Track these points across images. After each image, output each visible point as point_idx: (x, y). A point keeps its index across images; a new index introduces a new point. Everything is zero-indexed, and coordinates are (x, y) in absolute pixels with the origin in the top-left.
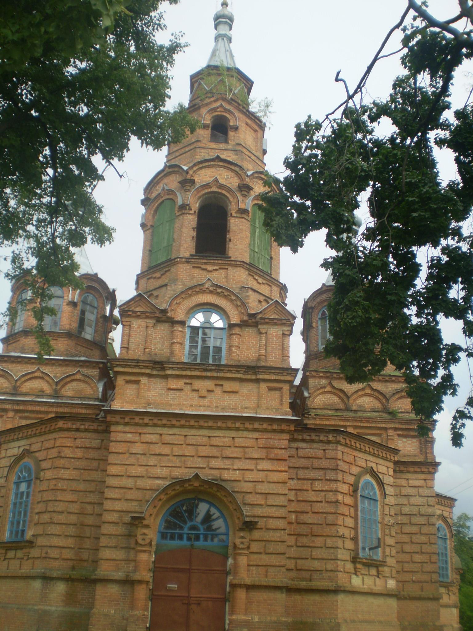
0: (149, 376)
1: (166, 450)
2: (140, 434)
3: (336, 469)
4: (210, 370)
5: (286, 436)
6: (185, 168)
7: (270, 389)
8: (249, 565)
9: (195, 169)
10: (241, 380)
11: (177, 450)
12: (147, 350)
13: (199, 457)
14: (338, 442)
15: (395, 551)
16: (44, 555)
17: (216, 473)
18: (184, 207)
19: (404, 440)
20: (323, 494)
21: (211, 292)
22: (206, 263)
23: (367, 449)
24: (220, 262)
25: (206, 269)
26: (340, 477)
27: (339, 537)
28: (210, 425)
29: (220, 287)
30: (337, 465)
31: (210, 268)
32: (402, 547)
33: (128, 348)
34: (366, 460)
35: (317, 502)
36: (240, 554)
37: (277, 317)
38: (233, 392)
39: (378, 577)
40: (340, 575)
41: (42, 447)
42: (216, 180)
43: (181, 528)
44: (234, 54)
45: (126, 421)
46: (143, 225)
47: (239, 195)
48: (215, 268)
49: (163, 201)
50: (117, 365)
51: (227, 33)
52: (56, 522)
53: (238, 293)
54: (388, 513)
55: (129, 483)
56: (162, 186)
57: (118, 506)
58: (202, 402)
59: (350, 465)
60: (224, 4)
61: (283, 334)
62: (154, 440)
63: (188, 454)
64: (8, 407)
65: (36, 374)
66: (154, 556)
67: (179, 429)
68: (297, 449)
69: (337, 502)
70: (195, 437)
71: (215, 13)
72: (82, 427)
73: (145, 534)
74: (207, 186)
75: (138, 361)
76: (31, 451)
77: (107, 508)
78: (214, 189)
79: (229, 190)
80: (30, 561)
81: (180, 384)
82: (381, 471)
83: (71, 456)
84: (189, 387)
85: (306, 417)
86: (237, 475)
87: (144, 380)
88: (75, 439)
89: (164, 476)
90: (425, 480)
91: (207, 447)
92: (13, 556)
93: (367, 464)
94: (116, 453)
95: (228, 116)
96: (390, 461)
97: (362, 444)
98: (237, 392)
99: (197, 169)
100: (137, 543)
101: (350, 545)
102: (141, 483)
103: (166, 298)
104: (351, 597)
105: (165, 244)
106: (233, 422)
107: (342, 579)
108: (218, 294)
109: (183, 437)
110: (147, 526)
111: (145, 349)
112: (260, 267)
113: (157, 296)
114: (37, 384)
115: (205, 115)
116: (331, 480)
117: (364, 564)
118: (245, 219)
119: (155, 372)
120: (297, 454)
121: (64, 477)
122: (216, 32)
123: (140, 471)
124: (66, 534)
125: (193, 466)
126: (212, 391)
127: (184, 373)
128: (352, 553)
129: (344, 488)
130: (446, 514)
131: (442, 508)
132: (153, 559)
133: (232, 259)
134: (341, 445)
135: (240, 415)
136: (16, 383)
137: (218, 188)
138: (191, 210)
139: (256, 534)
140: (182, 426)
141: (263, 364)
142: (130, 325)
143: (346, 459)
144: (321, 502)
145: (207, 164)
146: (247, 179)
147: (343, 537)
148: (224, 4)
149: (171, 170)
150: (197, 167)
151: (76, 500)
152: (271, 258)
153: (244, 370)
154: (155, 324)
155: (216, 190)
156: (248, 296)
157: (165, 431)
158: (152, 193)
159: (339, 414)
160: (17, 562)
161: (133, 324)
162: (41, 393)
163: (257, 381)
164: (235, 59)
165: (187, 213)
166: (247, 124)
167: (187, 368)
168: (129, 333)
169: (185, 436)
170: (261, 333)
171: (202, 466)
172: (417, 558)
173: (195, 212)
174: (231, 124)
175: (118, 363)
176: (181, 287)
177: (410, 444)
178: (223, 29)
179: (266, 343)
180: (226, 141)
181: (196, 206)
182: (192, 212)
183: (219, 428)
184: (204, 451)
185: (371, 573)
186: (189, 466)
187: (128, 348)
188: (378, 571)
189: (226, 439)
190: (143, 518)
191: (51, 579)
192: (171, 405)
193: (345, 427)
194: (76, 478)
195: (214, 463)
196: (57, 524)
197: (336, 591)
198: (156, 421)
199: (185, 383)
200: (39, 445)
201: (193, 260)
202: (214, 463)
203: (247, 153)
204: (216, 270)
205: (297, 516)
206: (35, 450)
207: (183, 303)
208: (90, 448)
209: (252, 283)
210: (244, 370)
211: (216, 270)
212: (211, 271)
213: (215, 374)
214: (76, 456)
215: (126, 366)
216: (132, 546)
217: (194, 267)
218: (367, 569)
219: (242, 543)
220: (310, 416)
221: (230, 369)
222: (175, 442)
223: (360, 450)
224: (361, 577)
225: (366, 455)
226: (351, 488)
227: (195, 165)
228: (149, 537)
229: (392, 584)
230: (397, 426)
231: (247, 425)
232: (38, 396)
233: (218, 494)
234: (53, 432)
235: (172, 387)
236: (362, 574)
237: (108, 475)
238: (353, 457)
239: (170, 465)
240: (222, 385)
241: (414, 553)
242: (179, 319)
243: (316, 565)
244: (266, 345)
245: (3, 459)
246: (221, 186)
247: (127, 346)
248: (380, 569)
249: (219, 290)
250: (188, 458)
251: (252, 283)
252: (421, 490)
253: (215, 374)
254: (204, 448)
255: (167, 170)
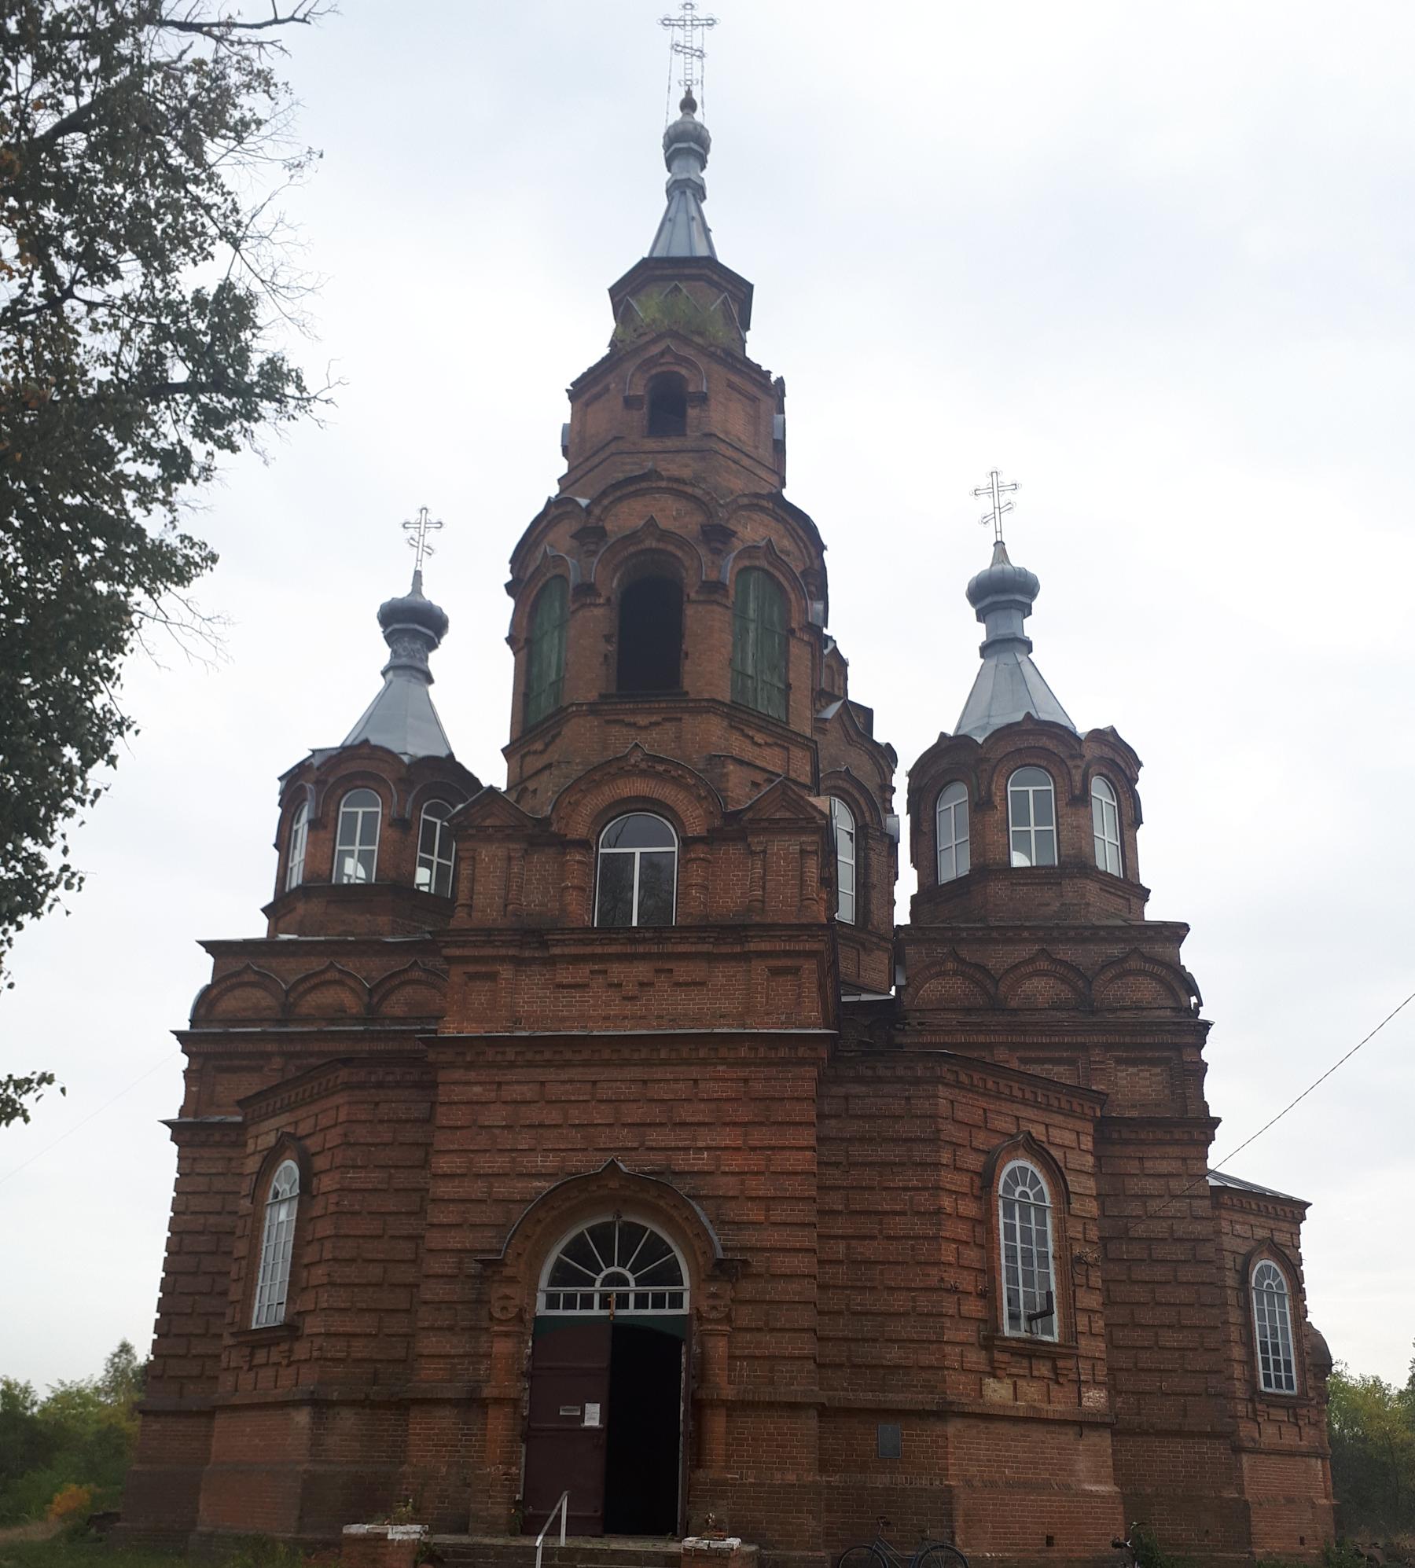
0: (518, 962)
1: (553, 1116)
2: (500, 1084)
3: (935, 1140)
4: (644, 940)
5: (812, 1072)
6: (584, 502)
7: (776, 972)
8: (732, 1357)
9: (606, 502)
10: (710, 958)
11: (576, 1115)
12: (510, 907)
13: (624, 1125)
14: (940, 1080)
15: (1101, 1323)
16: (315, 1354)
17: (659, 1158)
18: (586, 590)
19: (1131, 1070)
20: (906, 1196)
21: (643, 773)
22: (633, 712)
23: (1017, 1093)
24: (663, 705)
25: (634, 724)
26: (945, 1157)
27: (947, 1290)
28: (781, 1054)
29: (662, 761)
30: (938, 1131)
31: (642, 720)
32: (1133, 1314)
33: (470, 906)
34: (1017, 1118)
35: (895, 1213)
36: (711, 1333)
37: (788, 815)
38: (695, 984)
39: (1058, 1383)
40: (952, 1377)
41: (316, 1126)
42: (651, 522)
43: (592, 1283)
44: (709, 225)
45: (468, 1059)
46: (510, 640)
47: (702, 551)
48: (654, 719)
49: (547, 582)
50: (447, 944)
51: (693, 177)
52: (339, 1281)
53: (700, 771)
54: (1080, 1236)
55: (478, 1189)
56: (542, 550)
57: (456, 1240)
58: (629, 1008)
59: (974, 1130)
60: (688, 105)
61: (802, 852)
62: (529, 1096)
63: (600, 1121)
64: (270, 1047)
65: (329, 976)
66: (530, 1344)
67: (580, 1070)
68: (846, 1098)
69: (939, 1211)
70: (614, 1085)
71: (663, 131)
72: (390, 1078)
73: (507, 1297)
74: (633, 537)
75: (489, 932)
76: (298, 1135)
77: (433, 1246)
78: (651, 543)
79: (682, 542)
80: (292, 1370)
81: (582, 973)
82: (1058, 1141)
83: (370, 1140)
84: (600, 979)
85: (900, 1030)
86: (704, 1161)
87: (506, 972)
88: (377, 1104)
89: (550, 1171)
90: (1184, 1159)
91: (641, 1104)
92: (264, 1361)
93: (1018, 1125)
94: (450, 1128)
95: (683, 372)
96: (1082, 1117)
97: (1002, 1082)
98: (702, 984)
99: (612, 503)
100: (491, 1318)
101: (973, 1307)
102: (501, 1189)
103: (550, 794)
104: (982, 1426)
105: (553, 677)
106: (693, 1047)
107: (958, 1387)
108: (658, 775)
109: (589, 1086)
110: (512, 1280)
111: (506, 906)
112: (760, 709)
113: (535, 791)
114: (327, 997)
115: (633, 375)
116: (923, 1165)
117: (1014, 1353)
118: (719, 604)
119: (527, 954)
120: (847, 1110)
121: (354, 1186)
122: (669, 175)
123: (501, 1162)
124: (359, 1305)
125: (612, 1146)
126: (651, 984)
127: (588, 950)
128: (982, 1326)
129: (961, 1182)
130: (1279, 1237)
131: (1271, 1223)
132: (529, 1351)
133: (692, 696)
134: (946, 1085)
135: (709, 1031)
136: (287, 996)
137: (658, 540)
138: (600, 596)
139: (747, 1289)
140: (586, 1064)
141: (757, 919)
142: (474, 858)
143: (960, 1115)
144: (903, 1213)
145: (632, 489)
146: (722, 513)
147: (954, 1290)
148: (688, 105)
149: (560, 511)
150: (611, 498)
151: (380, 1232)
152: (789, 686)
153: (715, 935)
154: (526, 850)
155: (654, 544)
156: (726, 775)
157: (550, 1074)
158: (527, 566)
159: (974, 1019)
160: (270, 1372)
161: (480, 853)
162: (338, 1015)
163: (746, 957)
164: (714, 236)
165: (591, 604)
166: (731, 385)
167: (594, 940)
168: (473, 874)
169: (594, 1083)
170: (753, 853)
171: (629, 1145)
172: (1171, 1339)
173: (608, 600)
174: (691, 389)
175: (449, 939)
176: (580, 767)
177: (1145, 1079)
178: (686, 169)
179: (764, 874)
180: (681, 433)
181: (611, 585)
182: (602, 601)
183: (665, 1063)
184: (634, 1113)
185: (1036, 1373)
186: (602, 1146)
187: (470, 906)
188: (1054, 1368)
189: (681, 1085)
190: (501, 1263)
191: (331, 1404)
192: (563, 1019)
193: (990, 1046)
194: (380, 1186)
195: (655, 1138)
196: (340, 1285)
197: (943, 1413)
198: (568, 1055)
199: (592, 972)
200: (312, 1121)
201: (606, 707)
202: (655, 1138)
203: (730, 452)
204: (657, 724)
205: (848, 1248)
206: (304, 1134)
207: (584, 801)
208: (407, 1121)
209: (737, 745)
210: (715, 935)
211: (657, 724)
212: (645, 728)
213: (655, 949)
214: (378, 1140)
215: (463, 945)
216: (485, 1324)
217: (608, 722)
218: (1025, 1363)
219: (714, 1308)
220: (907, 1027)
221: (684, 935)
222: (573, 1098)
223: (998, 1096)
224: (1008, 1381)
225: (1015, 1105)
226: (978, 1182)
227: (604, 494)
228: (517, 1302)
229: (1094, 1398)
230: (1111, 1039)
231: (724, 1052)
232: (332, 1021)
233: (662, 1203)
234: (333, 1094)
235: (565, 981)
236: (1010, 1375)
237: (435, 1175)
238: (981, 1112)
239: (563, 1147)
240: (671, 971)
241: (1161, 1326)
242: (573, 835)
243: (893, 1355)
244: (763, 878)
245: (251, 1158)
246: (664, 535)
247: (469, 902)
248: (1060, 1364)
249: (661, 768)
250: (600, 1129)
251: (737, 745)
252: (1174, 1184)
253: (655, 949)
254: (635, 1106)
255: (554, 512)
